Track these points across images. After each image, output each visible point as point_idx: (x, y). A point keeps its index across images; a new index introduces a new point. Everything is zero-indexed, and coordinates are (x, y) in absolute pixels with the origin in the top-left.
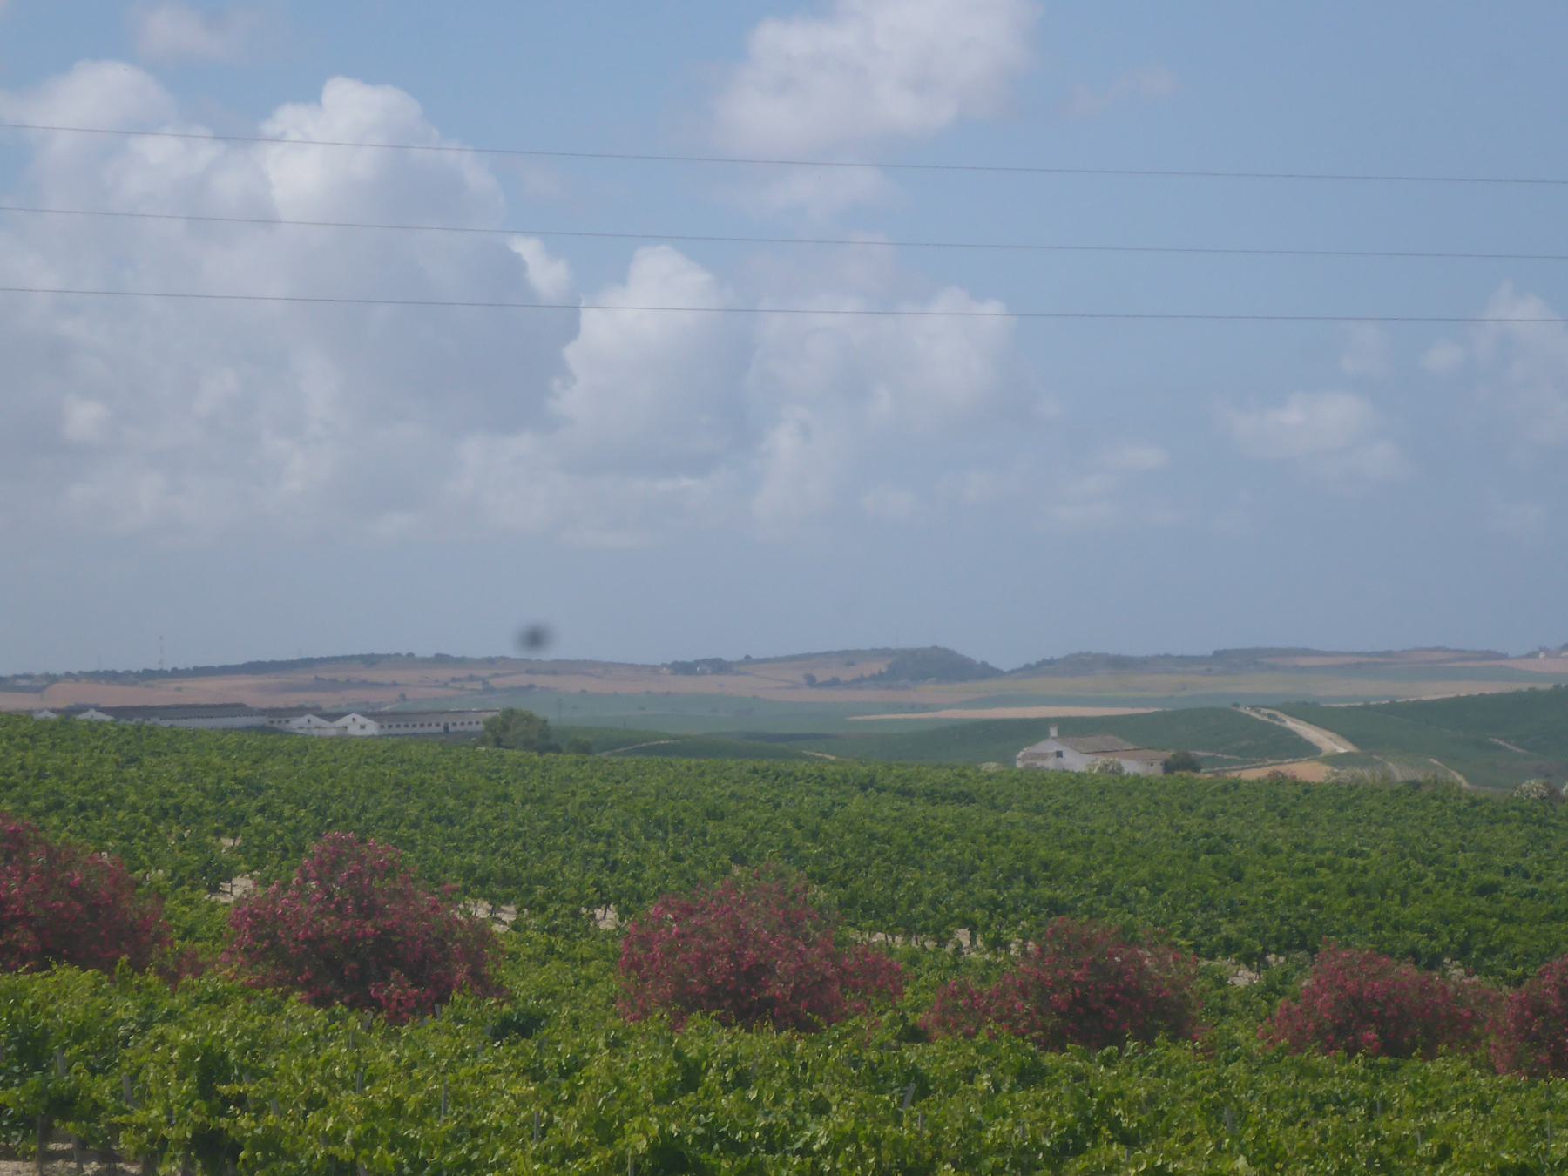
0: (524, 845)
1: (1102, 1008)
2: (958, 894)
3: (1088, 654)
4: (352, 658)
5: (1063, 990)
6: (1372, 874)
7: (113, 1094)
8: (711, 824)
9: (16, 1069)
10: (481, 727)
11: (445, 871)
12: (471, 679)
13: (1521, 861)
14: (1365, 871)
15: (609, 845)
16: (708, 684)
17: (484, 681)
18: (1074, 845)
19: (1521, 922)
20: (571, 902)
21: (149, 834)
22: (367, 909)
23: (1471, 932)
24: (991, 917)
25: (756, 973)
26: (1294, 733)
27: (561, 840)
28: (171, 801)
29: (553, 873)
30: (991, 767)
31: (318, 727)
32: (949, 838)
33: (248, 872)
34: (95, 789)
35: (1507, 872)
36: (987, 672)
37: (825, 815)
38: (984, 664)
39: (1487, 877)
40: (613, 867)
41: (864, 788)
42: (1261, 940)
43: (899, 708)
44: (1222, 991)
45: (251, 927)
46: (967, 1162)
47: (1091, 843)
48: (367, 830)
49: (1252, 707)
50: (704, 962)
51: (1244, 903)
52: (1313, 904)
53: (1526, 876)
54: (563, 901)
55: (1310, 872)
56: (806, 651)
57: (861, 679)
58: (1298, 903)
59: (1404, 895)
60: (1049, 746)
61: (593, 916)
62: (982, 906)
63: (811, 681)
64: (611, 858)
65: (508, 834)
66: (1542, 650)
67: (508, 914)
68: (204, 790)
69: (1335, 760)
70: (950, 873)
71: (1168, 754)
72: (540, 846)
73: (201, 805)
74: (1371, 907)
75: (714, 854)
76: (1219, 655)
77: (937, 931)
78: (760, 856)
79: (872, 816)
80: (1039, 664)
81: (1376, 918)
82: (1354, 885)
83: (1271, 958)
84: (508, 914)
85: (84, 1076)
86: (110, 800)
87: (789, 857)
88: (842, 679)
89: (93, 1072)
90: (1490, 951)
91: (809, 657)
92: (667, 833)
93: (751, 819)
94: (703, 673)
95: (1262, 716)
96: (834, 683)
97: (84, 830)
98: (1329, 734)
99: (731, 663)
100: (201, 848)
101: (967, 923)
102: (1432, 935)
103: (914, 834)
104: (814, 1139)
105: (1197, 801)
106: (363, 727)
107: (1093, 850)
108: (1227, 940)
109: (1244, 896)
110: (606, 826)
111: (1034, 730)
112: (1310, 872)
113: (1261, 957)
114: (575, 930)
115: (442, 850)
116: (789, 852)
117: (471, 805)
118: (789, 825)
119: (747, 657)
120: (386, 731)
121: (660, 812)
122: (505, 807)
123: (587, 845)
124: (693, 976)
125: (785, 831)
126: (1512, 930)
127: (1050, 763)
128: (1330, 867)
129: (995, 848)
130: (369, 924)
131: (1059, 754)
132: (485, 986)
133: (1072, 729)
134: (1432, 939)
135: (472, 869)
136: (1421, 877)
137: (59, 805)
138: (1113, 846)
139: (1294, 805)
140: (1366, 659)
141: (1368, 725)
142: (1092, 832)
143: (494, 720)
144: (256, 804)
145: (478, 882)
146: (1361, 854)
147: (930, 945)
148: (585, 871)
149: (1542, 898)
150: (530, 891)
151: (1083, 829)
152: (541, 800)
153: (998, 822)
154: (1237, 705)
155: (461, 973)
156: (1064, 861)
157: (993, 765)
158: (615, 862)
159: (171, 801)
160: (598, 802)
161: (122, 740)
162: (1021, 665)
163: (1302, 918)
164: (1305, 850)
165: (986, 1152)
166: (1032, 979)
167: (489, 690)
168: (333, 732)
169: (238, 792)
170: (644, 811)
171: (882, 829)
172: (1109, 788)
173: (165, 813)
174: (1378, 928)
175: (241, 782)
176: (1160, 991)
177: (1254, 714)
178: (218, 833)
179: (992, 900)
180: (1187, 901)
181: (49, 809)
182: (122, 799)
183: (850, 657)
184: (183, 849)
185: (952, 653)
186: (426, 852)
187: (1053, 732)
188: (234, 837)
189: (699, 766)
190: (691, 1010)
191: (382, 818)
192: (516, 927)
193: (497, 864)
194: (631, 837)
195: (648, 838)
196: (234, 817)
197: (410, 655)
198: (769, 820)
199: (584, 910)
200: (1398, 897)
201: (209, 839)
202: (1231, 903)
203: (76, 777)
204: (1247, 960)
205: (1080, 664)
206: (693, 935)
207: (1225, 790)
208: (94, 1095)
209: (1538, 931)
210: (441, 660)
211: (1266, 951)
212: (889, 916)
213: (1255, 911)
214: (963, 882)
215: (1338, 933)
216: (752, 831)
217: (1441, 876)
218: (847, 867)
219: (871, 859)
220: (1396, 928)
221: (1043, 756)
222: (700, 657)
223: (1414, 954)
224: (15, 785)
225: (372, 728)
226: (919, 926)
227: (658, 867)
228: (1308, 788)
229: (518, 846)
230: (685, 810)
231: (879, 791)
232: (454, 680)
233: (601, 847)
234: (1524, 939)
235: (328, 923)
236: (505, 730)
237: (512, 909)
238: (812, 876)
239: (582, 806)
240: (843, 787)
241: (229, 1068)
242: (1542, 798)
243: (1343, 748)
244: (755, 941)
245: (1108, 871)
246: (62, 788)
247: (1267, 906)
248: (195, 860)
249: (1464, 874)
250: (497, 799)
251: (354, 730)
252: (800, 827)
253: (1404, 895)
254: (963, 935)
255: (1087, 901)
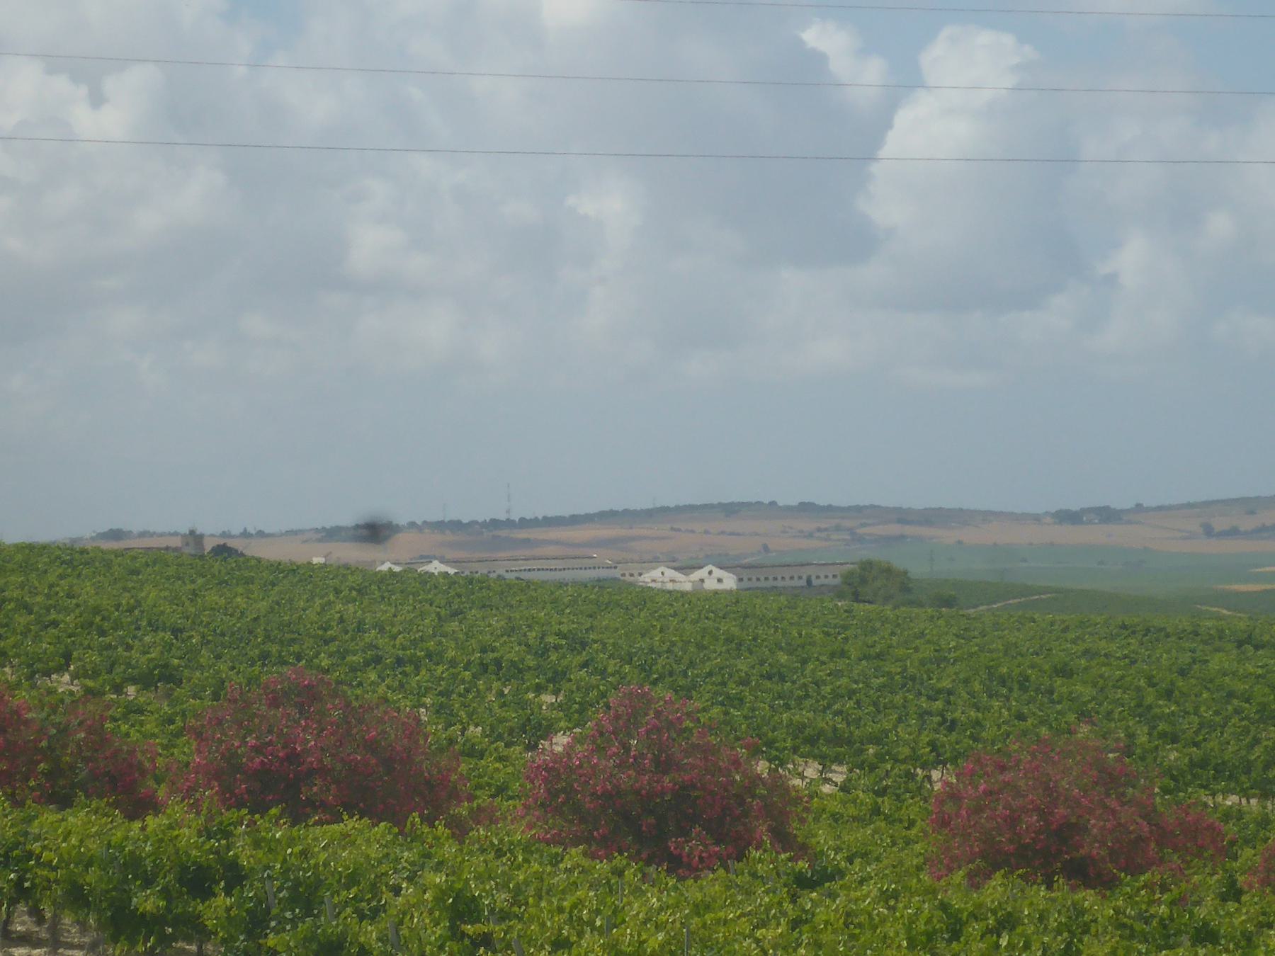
0: (858, 702)
4: (1218, 501)
7: (379, 939)
9: (288, 915)
11: (774, 730)
12: (838, 529)
16: (1095, 534)
20: (904, 761)
21: (467, 690)
22: (664, 765)
25: (1066, 833)
27: (898, 699)
28: (492, 655)
29: (886, 733)
31: (672, 581)
33: (569, 729)
34: (414, 643)
37: (1183, 673)
40: (952, 726)
41: (1240, 644)
45: (545, 780)
48: (694, 687)
50: (1012, 821)
54: (896, 761)
56: (1204, 499)
61: (929, 778)
63: (1209, 531)
64: (949, 716)
67: (839, 774)
68: (527, 645)
72: (875, 704)
73: (522, 661)
75: (1059, 713)
79: (1234, 674)
84: (839, 774)
85: (353, 921)
86: (429, 656)
88: (1242, 529)
89: (362, 917)
92: (1011, 690)
94: (1090, 522)
96: (1233, 532)
97: (402, 685)
99: (1122, 511)
100: (522, 704)
106: (720, 580)
110: (946, 684)
115: (772, 707)
116: (1142, 711)
117: (804, 662)
118: (1142, 683)
120: (746, 584)
122: (841, 664)
125: (1138, 689)
130: (667, 779)
132: (783, 839)
135: (802, 727)
137: (378, 660)
143: (851, 573)
144: (580, 659)
145: (810, 742)
152: (879, 656)
155: (762, 829)
158: (954, 722)
159: (492, 655)
160: (940, 660)
161: (453, 593)
168: (688, 587)
169: (561, 647)
171: (1241, 687)
173: (484, 668)
175: (564, 637)
178: (539, 689)
181: (367, 664)
182: (441, 654)
184: (503, 705)
186: (753, 710)
188: (556, 693)
189: (1064, 621)
190: (996, 867)
191: (710, 674)
192: (844, 788)
193: (825, 722)
194: (972, 694)
195: (990, 696)
196: (556, 672)
197: (773, 503)
198: (1122, 677)
199: (919, 771)
201: (531, 695)
203: (395, 630)
206: (1000, 792)
208: (362, 939)
210: (806, 508)
212: (1243, 778)
216: (1102, 689)
218: (1201, 725)
222: (1086, 506)
224: (333, 639)
225: (730, 582)
227: (999, 727)
229: (851, 704)
230: (1032, 667)
231: (1257, 648)
232: (819, 530)
233: (939, 704)
235: (626, 779)
236: (864, 582)
237: (844, 769)
239: (923, 663)
240: (1218, 643)
241: (481, 911)
246: (381, 642)
248: (513, 717)
250: (833, 655)
251: (711, 585)
252: (1152, 685)
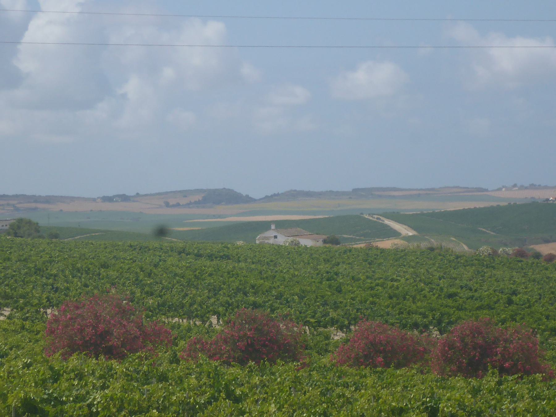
1: (260, 347)
2: (212, 300)
3: (295, 191)
5: (243, 341)
6: (401, 289)
8: (103, 270)
10: (8, 226)
12: (8, 205)
13: (468, 283)
14: (398, 288)
15: (55, 280)
17: (14, 206)
18: (267, 277)
19: (466, 309)
23: (442, 315)
24: (227, 310)
25: (105, 335)
26: (389, 226)
27: (33, 279)
29: (27, 293)
30: (240, 243)
32: (210, 275)
35: (462, 287)
36: (248, 200)
37: (156, 266)
38: (247, 196)
39: (453, 290)
40: (57, 290)
41: (180, 253)
42: (348, 319)
43: (208, 217)
44: (327, 342)
46: (162, 409)
47: (275, 277)
49: (369, 214)
51: (341, 302)
52: (373, 303)
53: (471, 290)
54: (32, 306)
55: (372, 288)
57: (190, 203)
58: (365, 302)
59: (414, 298)
60: (271, 233)
61: (46, 312)
62: (223, 306)
63: (167, 205)
65: (9, 276)
66: (503, 187)
69: (408, 239)
70: (209, 291)
71: (325, 237)
72: (23, 281)
74: (399, 304)
76: (355, 191)
77: (202, 317)
78: (124, 285)
79: (177, 266)
80: (272, 196)
81: (400, 309)
82: (392, 294)
83: (352, 327)
87: (137, 284)
88: (181, 204)
90: (450, 323)
91: (167, 193)
93: (121, 268)
94: (117, 201)
95: (374, 218)
96: (178, 205)
98: (405, 226)
101: (215, 313)
102: (425, 316)
103: (195, 273)
104: (94, 399)
105: (331, 258)
107: (276, 279)
108: (332, 319)
109: (341, 300)
110: (54, 272)
111: (265, 226)
112: (372, 288)
113: (348, 327)
114: (37, 318)
116: (137, 282)
118: (138, 270)
119: (138, 194)
121: (79, 265)
122: (8, 264)
123: (44, 280)
124: (76, 337)
125: (137, 273)
126: (462, 314)
127: (272, 241)
128: (382, 286)
129: (231, 279)
131: (276, 237)
133: (281, 225)
134: (424, 318)
136: (422, 290)
138: (284, 277)
139: (375, 259)
140: (415, 192)
141: (420, 221)
142: (276, 272)
146: (396, 280)
147: (198, 323)
148: (43, 292)
149: (476, 299)
150: (17, 302)
151: (272, 270)
152: (25, 260)
153: (234, 267)
154: (362, 214)
156: (261, 285)
157: (242, 242)
158: (57, 288)
162: (264, 196)
163: (367, 309)
164: (371, 278)
165: (172, 404)
166: (229, 336)
167: (17, 209)
170: (72, 265)
172: (297, 251)
174: (401, 313)
176: (285, 340)
177: (371, 218)
179: (227, 303)
180: (315, 302)
183: (185, 193)
185: (233, 191)
187: (273, 227)
194: (65, 276)
195: (73, 277)
199: (42, 310)
200: (411, 299)
202: (335, 302)
204: (341, 328)
205: (294, 195)
206: (75, 318)
207: (345, 252)
209: (473, 314)
211: (350, 324)
213: (346, 306)
214: (215, 295)
215: (382, 316)
217: (432, 290)
218: (163, 288)
219: (174, 286)
220: (409, 314)
221: (268, 238)
223: (416, 325)
226: (194, 315)
228: (383, 251)
231: (187, 255)
233: (51, 281)
234: (466, 318)
238: (147, 293)
242: (489, 254)
243: (411, 233)
244: (104, 321)
245: (281, 289)
247: (351, 304)
249: (442, 289)
252: (143, 271)
253: (414, 298)
254: (214, 319)
255: (270, 303)
